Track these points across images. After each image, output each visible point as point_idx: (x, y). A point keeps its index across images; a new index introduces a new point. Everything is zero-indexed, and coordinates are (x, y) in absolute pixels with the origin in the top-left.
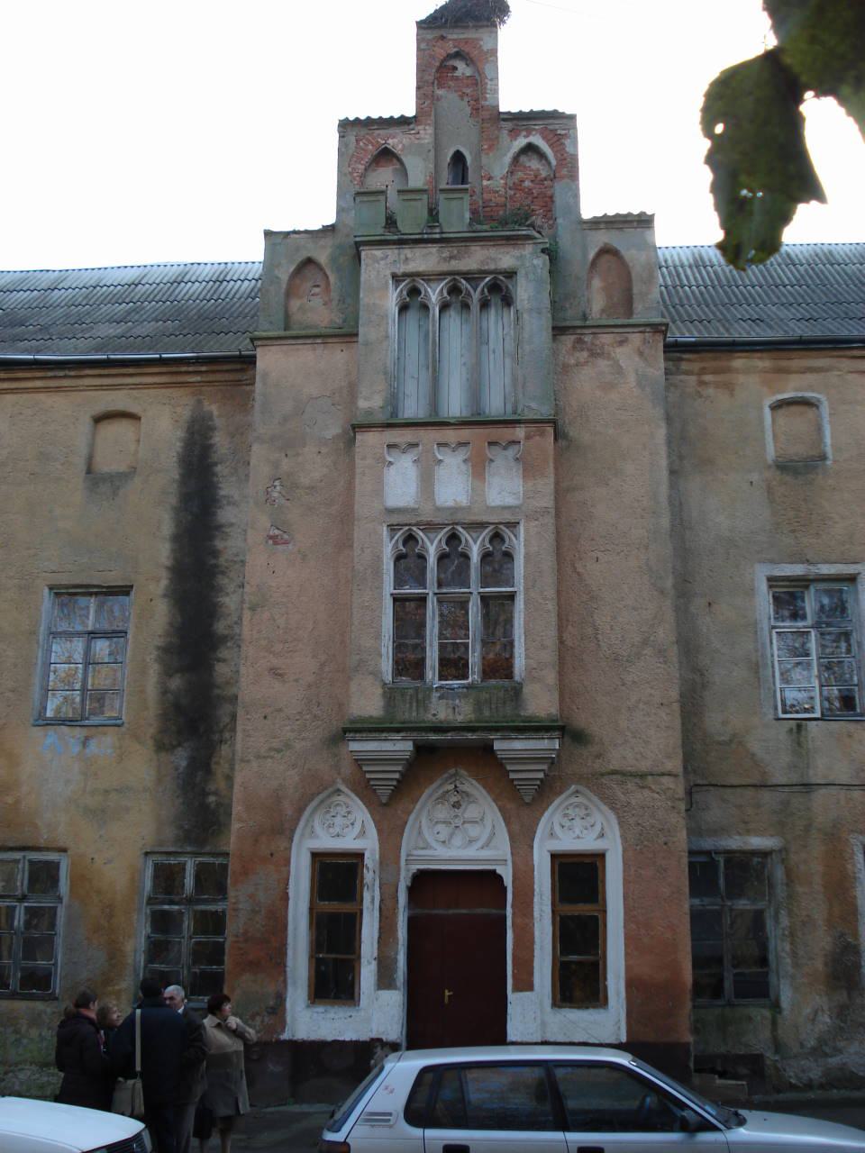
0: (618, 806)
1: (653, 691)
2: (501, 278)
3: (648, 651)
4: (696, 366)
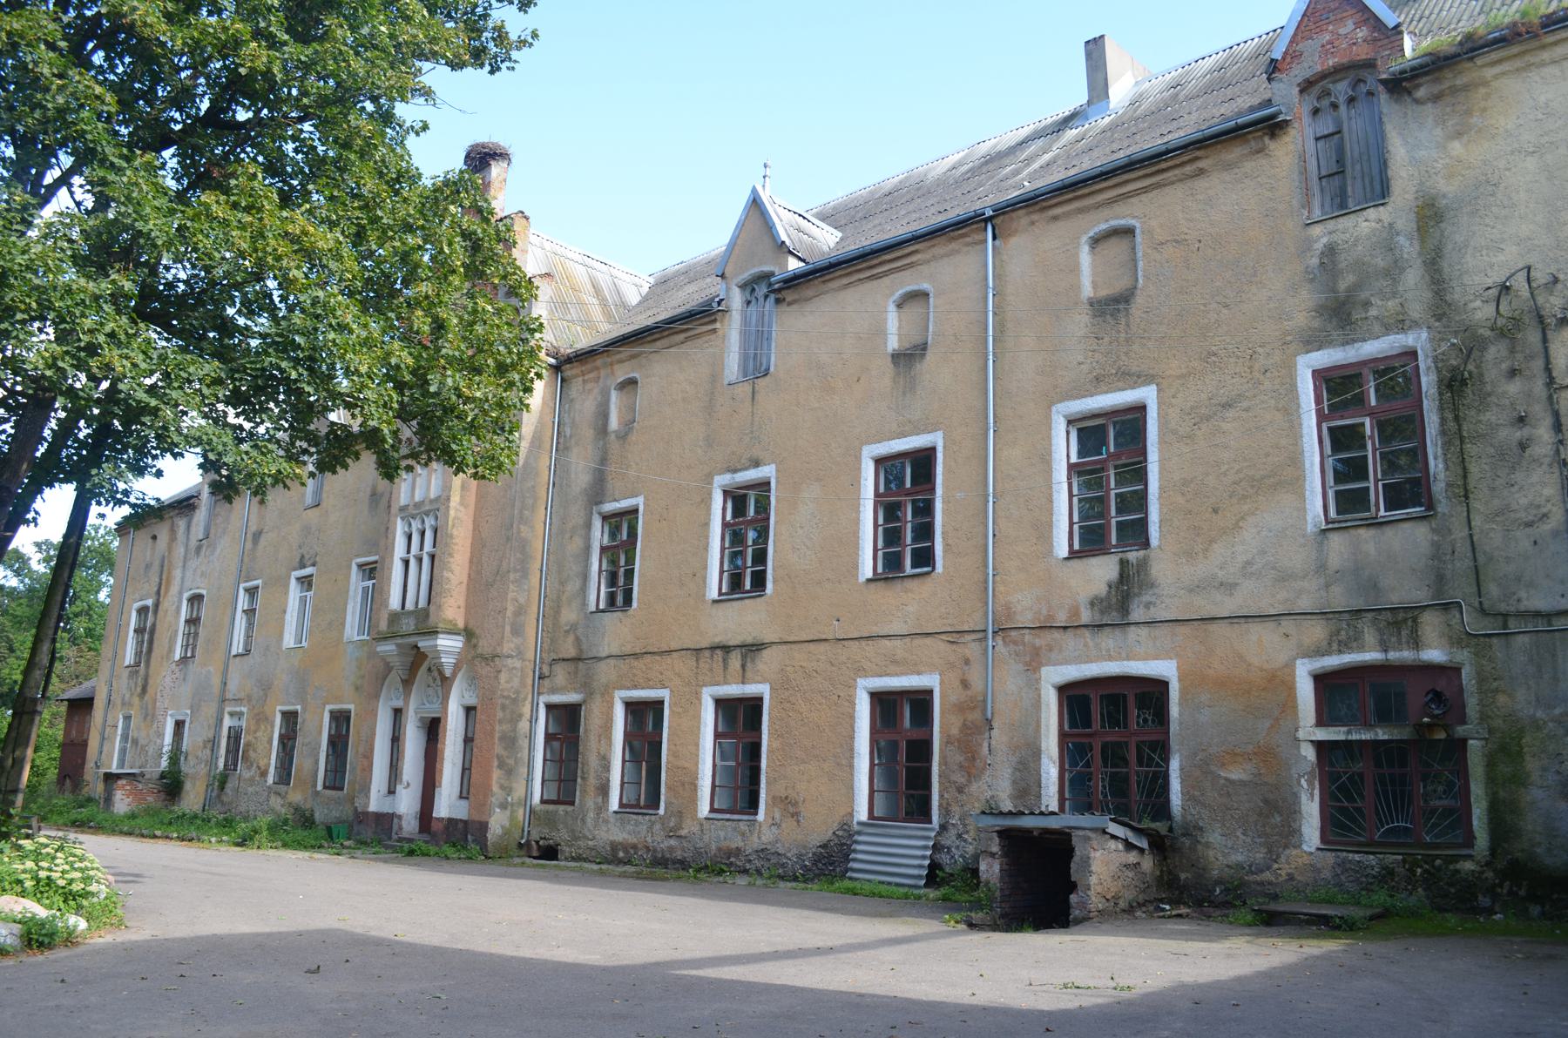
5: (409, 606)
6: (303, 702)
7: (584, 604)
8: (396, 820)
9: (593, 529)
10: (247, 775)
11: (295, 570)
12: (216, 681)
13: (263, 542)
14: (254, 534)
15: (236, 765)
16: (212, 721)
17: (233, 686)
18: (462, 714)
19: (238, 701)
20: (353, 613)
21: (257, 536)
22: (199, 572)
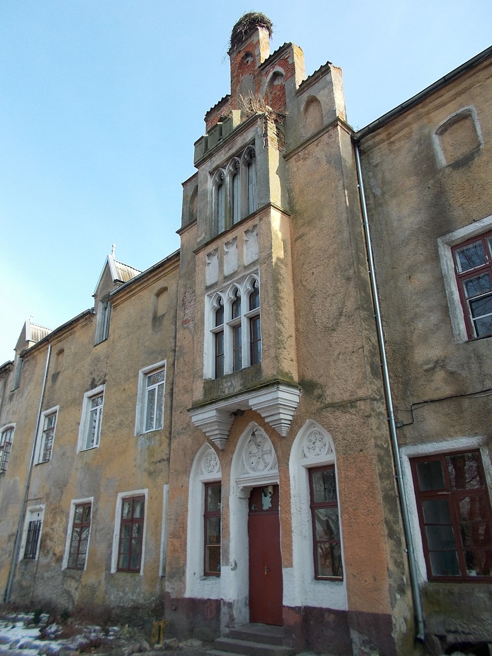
0: (332, 429)
1: (347, 345)
2: (250, 146)
3: (343, 319)
4: (383, 136)
5: (228, 368)
6: (96, 493)
7: (451, 335)
8: (224, 609)
9: (443, 261)
10: (44, 561)
11: (87, 390)
12: (21, 488)
13: (60, 378)
14: (53, 376)
15: (34, 554)
16: (17, 519)
17: (34, 490)
18: (304, 475)
19: (38, 500)
20: (142, 412)
21: (55, 376)
22: (11, 411)
